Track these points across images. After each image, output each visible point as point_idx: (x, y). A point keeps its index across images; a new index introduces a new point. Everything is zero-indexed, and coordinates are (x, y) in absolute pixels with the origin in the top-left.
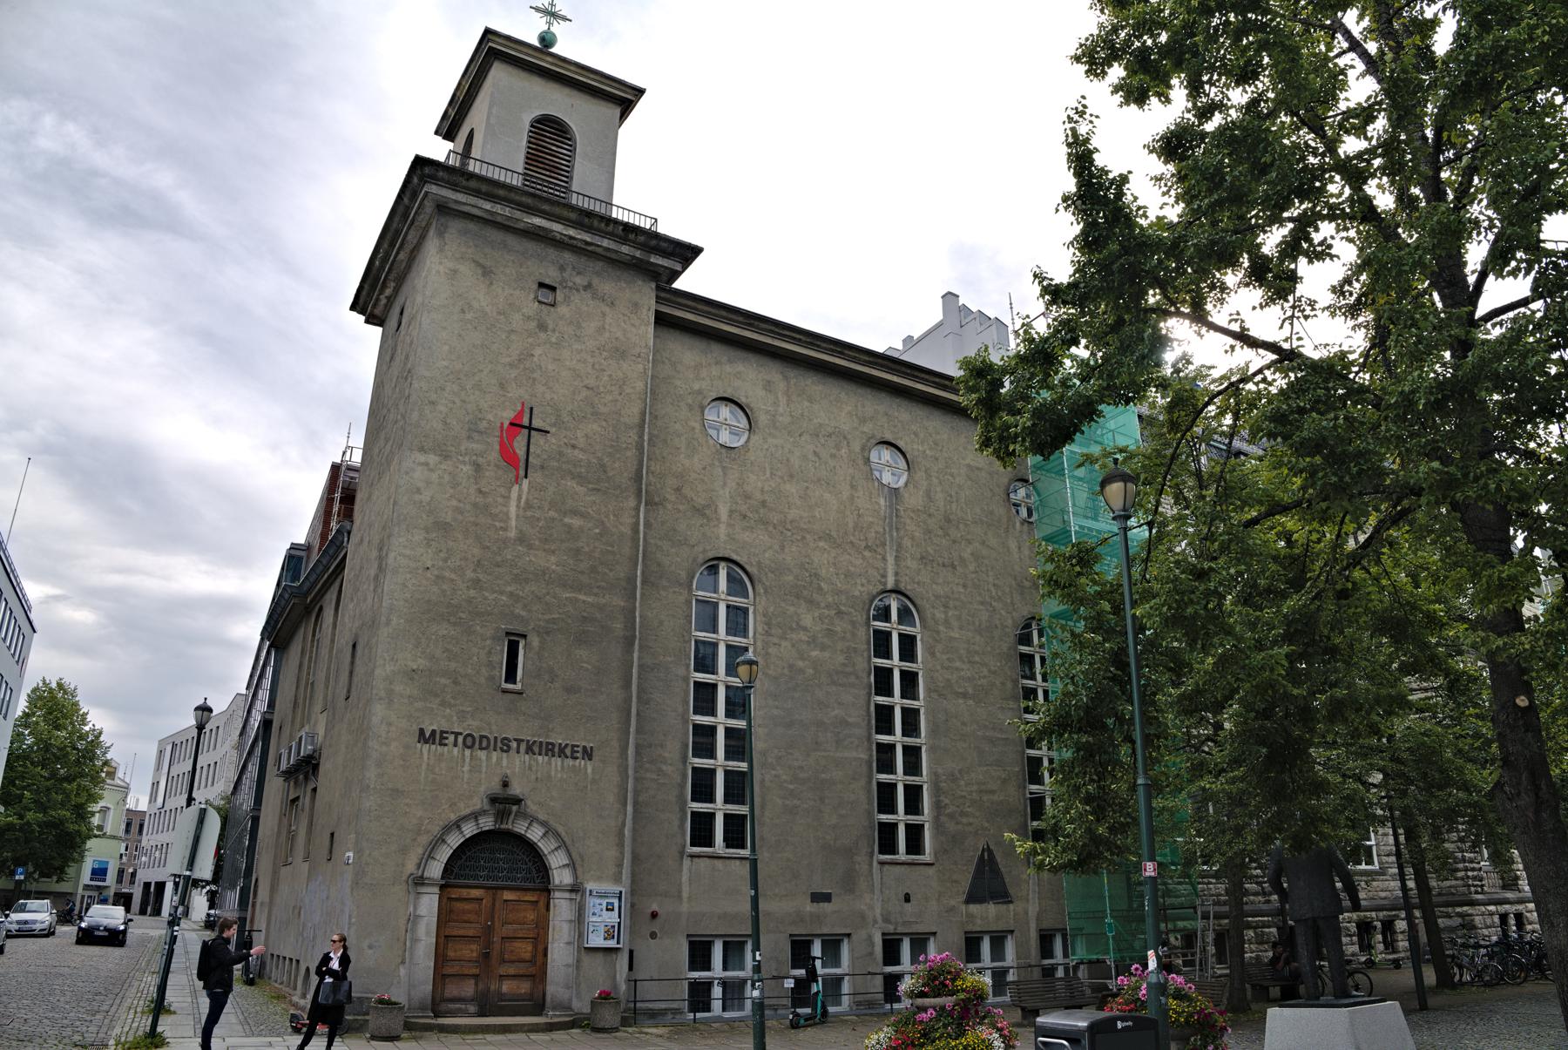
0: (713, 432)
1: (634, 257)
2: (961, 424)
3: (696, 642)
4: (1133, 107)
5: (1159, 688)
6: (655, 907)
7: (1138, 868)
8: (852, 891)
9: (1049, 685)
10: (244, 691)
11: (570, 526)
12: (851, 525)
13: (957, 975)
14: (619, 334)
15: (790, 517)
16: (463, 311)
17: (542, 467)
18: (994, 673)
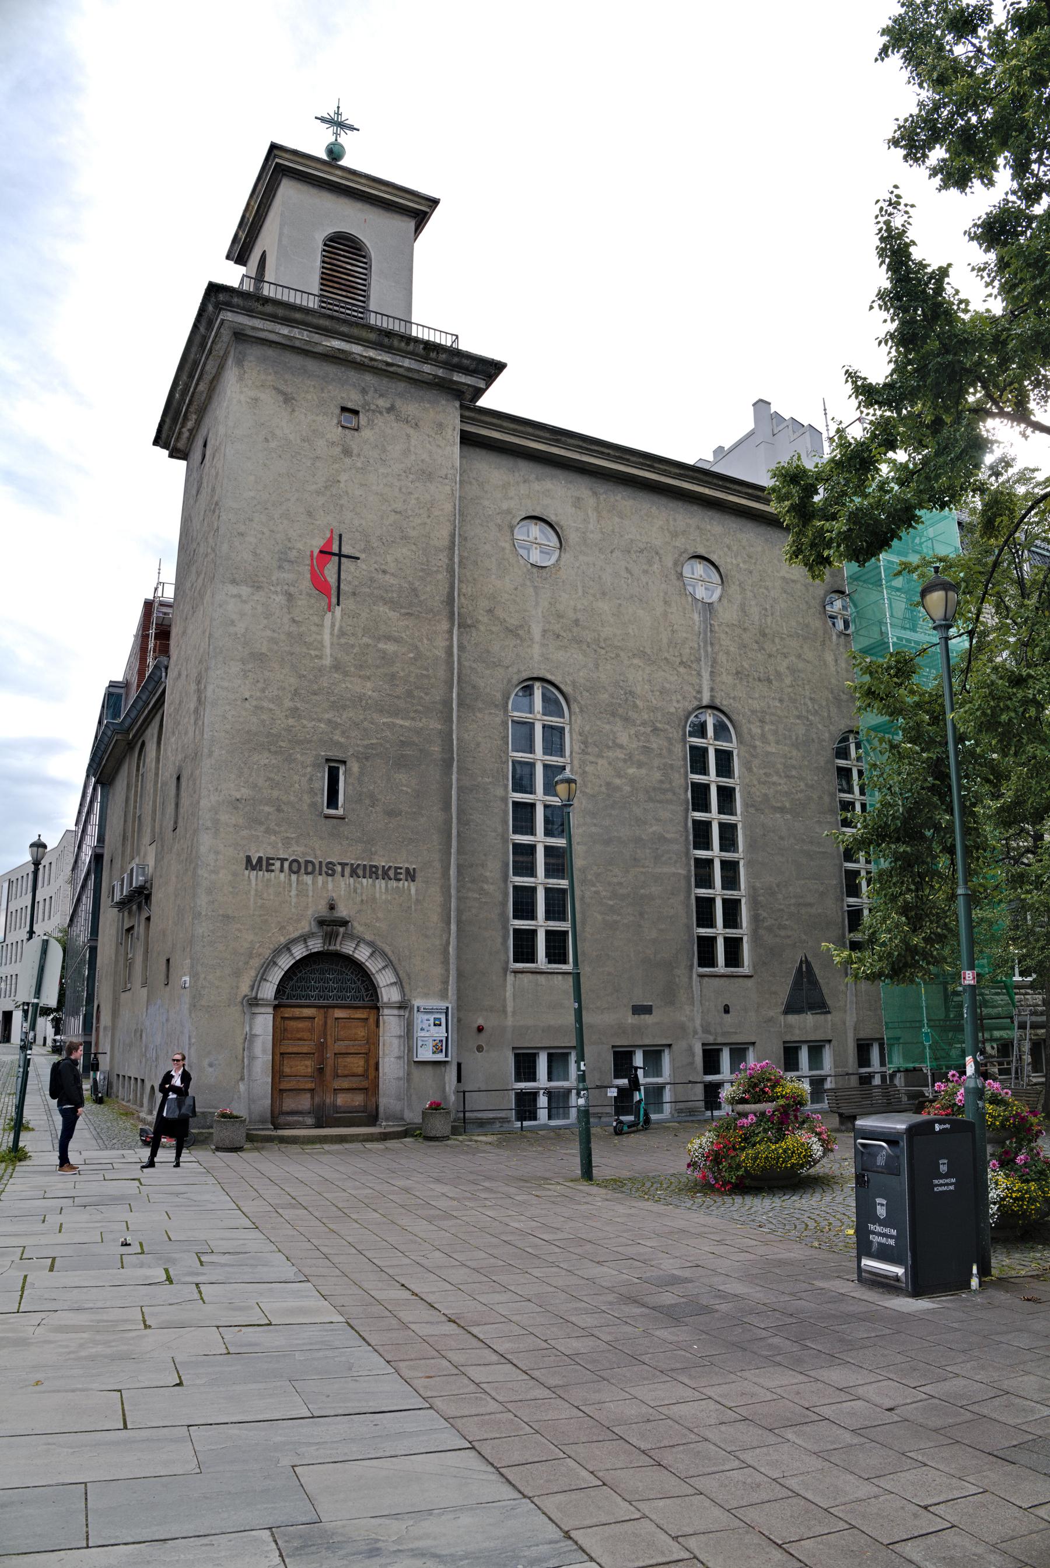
0: (521, 551)
1: (436, 376)
2: (774, 534)
3: (513, 762)
4: (954, 192)
5: (978, 800)
6: (480, 1022)
7: (957, 976)
8: (672, 1003)
9: (866, 799)
10: (73, 828)
11: (384, 652)
12: (665, 641)
13: (776, 1083)
14: (425, 456)
15: (603, 635)
16: (266, 440)
17: (354, 594)
18: (812, 786)
